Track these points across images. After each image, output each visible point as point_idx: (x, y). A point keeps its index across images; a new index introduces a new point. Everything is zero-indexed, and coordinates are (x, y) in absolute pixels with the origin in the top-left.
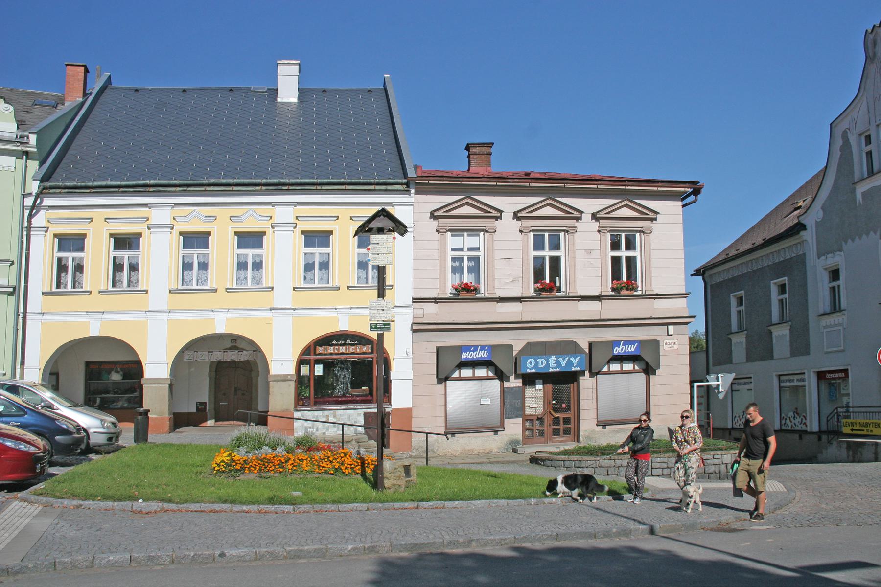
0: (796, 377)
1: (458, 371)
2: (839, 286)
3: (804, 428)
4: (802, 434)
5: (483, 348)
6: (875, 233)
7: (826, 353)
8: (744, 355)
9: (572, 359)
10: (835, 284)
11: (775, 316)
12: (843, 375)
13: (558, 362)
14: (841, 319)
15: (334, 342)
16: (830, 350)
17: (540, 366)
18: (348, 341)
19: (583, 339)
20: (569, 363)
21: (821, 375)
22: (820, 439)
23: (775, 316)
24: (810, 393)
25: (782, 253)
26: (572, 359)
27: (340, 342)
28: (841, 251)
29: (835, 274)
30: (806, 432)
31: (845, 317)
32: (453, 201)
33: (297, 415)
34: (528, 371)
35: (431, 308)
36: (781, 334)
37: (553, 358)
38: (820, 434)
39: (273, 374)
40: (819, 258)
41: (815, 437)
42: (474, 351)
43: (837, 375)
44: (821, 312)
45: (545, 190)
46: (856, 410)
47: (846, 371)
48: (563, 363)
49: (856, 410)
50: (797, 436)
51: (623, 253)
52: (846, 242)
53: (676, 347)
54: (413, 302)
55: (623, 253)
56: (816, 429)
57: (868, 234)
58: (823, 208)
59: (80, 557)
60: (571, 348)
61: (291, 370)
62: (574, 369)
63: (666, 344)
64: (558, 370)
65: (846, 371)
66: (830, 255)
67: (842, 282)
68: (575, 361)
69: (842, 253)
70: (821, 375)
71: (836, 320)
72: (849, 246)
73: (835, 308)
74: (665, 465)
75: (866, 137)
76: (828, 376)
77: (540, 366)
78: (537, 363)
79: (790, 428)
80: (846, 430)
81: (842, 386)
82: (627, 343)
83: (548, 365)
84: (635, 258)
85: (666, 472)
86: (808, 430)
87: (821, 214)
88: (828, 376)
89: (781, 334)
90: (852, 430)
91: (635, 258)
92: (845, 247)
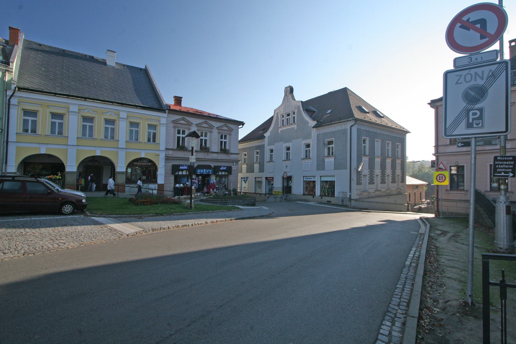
0: (260, 178)
1: (2, 183)
2: (273, 154)
3: (261, 193)
4: (261, 194)
5: (186, 166)
6: (301, 138)
7: (268, 172)
8: (333, 167)
9: (210, 170)
10: (288, 152)
11: (255, 161)
12: (272, 179)
13: (206, 171)
14: (273, 163)
15: (140, 161)
16: (305, 170)
17: (201, 172)
18: (144, 161)
19: (213, 165)
20: (209, 172)
21: (266, 178)
22: (265, 195)
23: (255, 161)
24: (263, 183)
25: (249, 145)
26: (210, 170)
27: (141, 161)
28: (291, 142)
29: (272, 151)
30: (262, 194)
31: (311, 161)
32: (474, 69)
33: (126, 185)
34: (198, 173)
35: (171, 152)
36: (256, 166)
37: (205, 170)
38: (265, 194)
39: (118, 171)
40: (268, 146)
41: (264, 195)
42: (183, 166)
43: (271, 178)
44: (284, 160)
45: (4, 148)
46: (275, 188)
47: (273, 178)
48: (207, 172)
49: (275, 188)
50: (259, 195)
51: (223, 140)
52: (275, 143)
53: (235, 168)
54: (166, 150)
55: (223, 140)
56: (264, 193)
57: (281, 142)
58: (270, 132)
59: (434, 253)
60: (208, 167)
61: (124, 170)
62: (210, 173)
63: (233, 167)
64: (206, 173)
65: (273, 178)
66: (271, 146)
67: (290, 151)
68: (210, 171)
69: (291, 143)
70: (266, 178)
71: (285, 162)
72: (276, 144)
73: (271, 161)
74: (238, 202)
75: (293, 112)
76: (268, 179)
77: (201, 172)
78: (200, 171)
79: (257, 192)
80: (274, 193)
81: (271, 181)
82: (224, 167)
83: (203, 172)
84: (226, 142)
85: (239, 204)
86: (262, 193)
87: (269, 134)
88: (268, 179)
89: (256, 166)
90: (275, 193)
91: (226, 142)
92: (275, 144)
